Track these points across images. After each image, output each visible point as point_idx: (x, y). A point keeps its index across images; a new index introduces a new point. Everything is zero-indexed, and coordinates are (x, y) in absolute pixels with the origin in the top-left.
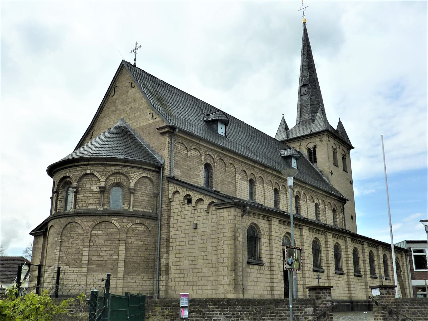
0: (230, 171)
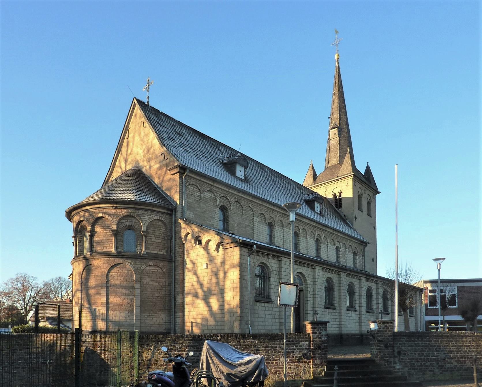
0: (247, 214)
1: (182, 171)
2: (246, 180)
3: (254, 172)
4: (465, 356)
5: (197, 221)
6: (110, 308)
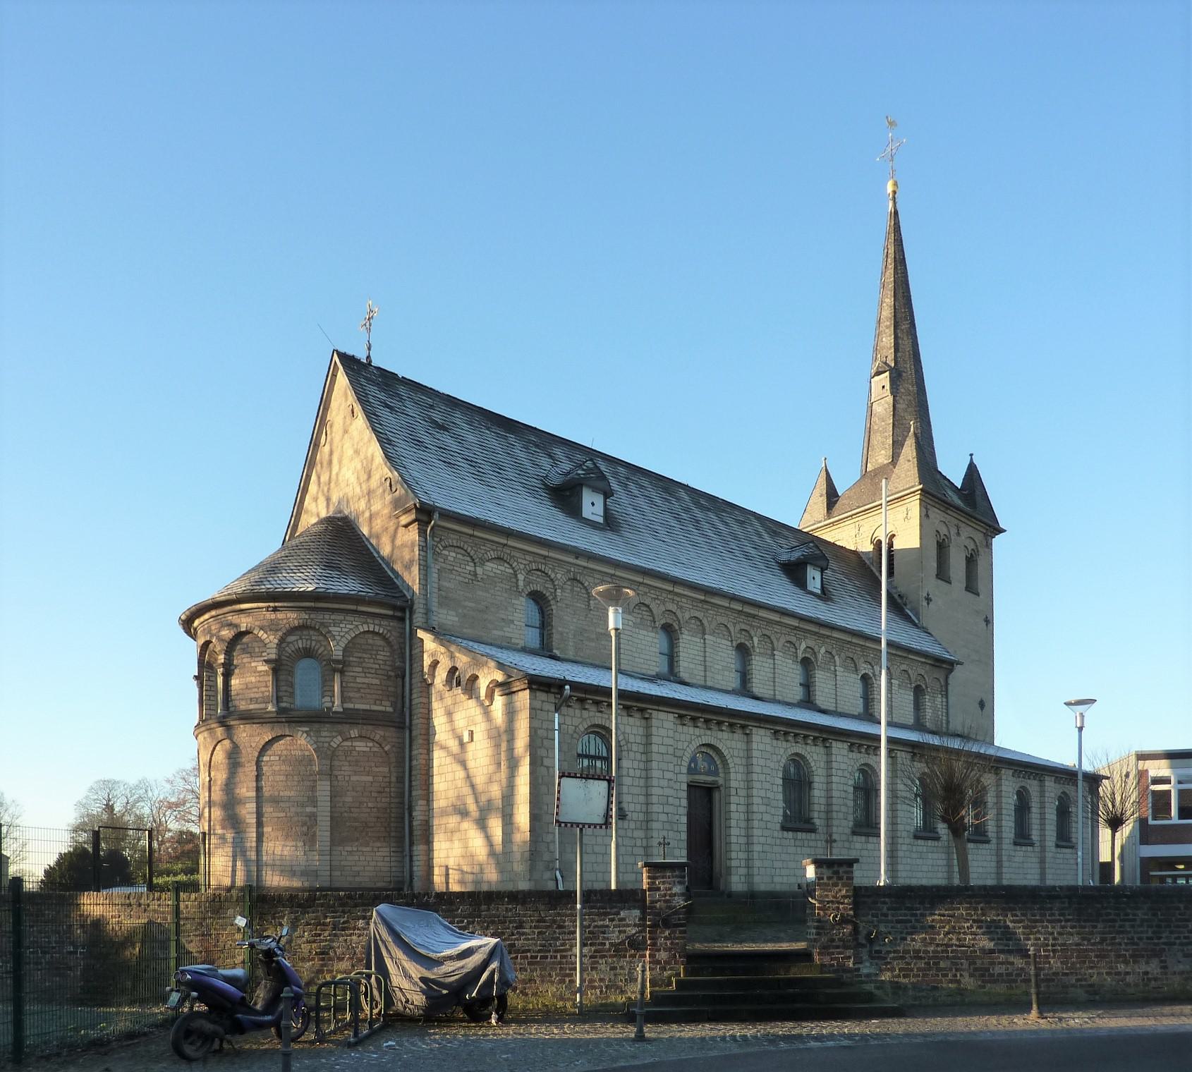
1: (425, 518)
2: (610, 523)
3: (641, 502)
4: (1047, 945)
5: (465, 630)
6: (266, 836)
